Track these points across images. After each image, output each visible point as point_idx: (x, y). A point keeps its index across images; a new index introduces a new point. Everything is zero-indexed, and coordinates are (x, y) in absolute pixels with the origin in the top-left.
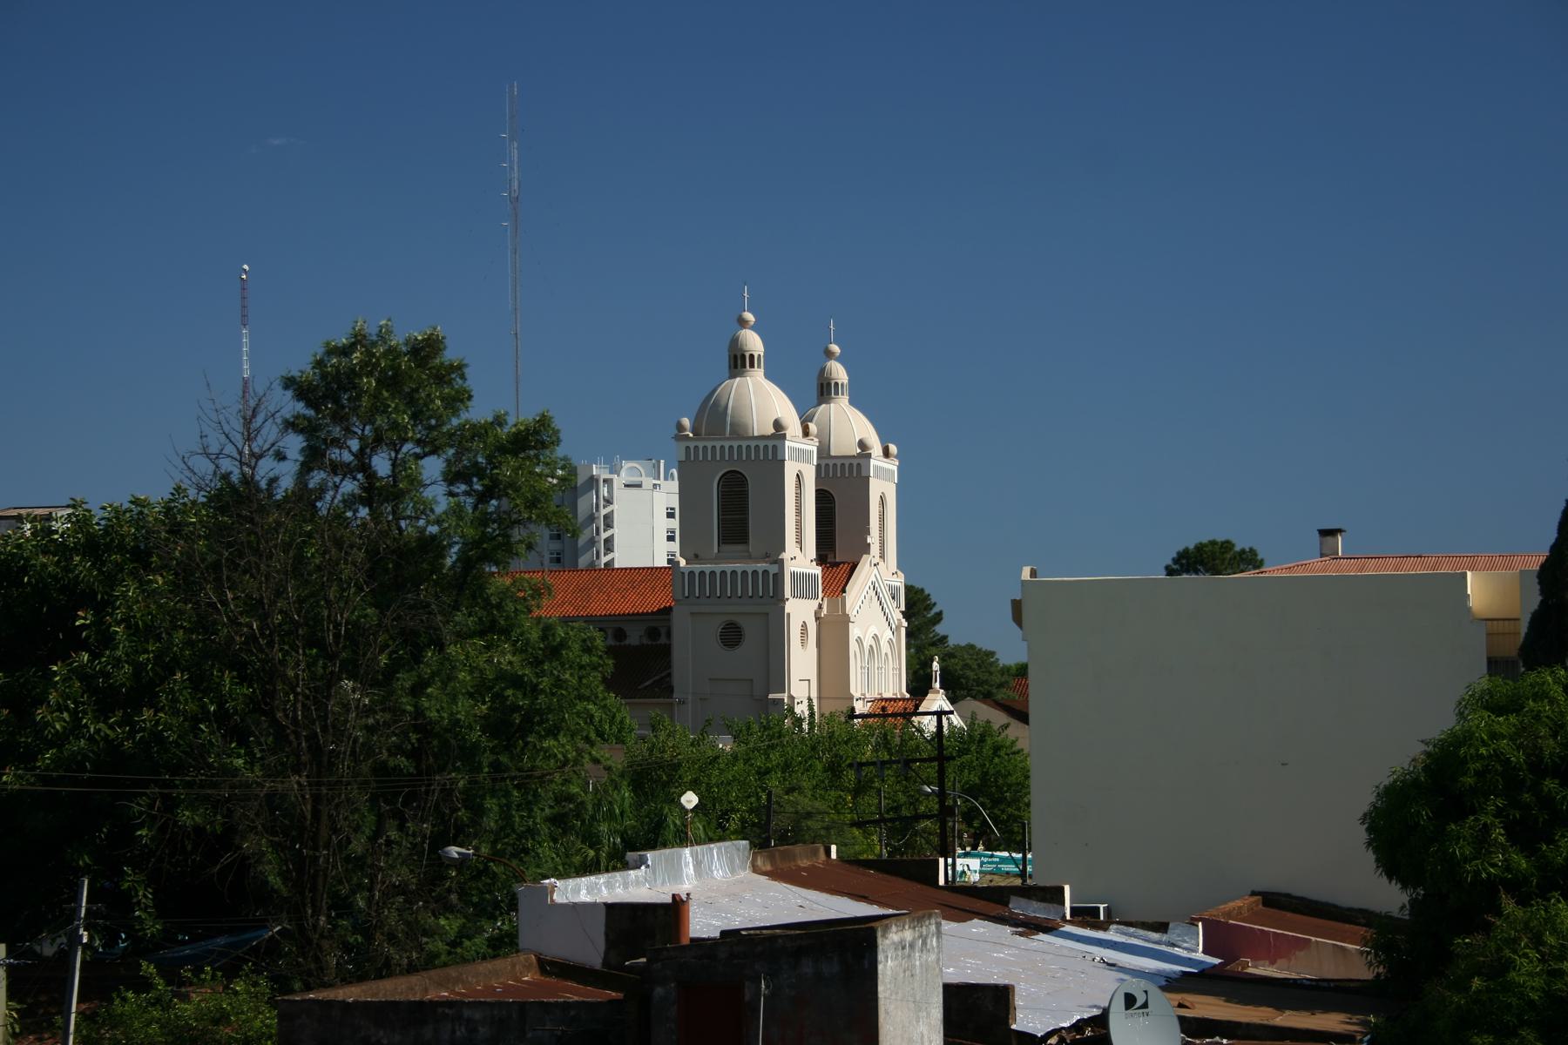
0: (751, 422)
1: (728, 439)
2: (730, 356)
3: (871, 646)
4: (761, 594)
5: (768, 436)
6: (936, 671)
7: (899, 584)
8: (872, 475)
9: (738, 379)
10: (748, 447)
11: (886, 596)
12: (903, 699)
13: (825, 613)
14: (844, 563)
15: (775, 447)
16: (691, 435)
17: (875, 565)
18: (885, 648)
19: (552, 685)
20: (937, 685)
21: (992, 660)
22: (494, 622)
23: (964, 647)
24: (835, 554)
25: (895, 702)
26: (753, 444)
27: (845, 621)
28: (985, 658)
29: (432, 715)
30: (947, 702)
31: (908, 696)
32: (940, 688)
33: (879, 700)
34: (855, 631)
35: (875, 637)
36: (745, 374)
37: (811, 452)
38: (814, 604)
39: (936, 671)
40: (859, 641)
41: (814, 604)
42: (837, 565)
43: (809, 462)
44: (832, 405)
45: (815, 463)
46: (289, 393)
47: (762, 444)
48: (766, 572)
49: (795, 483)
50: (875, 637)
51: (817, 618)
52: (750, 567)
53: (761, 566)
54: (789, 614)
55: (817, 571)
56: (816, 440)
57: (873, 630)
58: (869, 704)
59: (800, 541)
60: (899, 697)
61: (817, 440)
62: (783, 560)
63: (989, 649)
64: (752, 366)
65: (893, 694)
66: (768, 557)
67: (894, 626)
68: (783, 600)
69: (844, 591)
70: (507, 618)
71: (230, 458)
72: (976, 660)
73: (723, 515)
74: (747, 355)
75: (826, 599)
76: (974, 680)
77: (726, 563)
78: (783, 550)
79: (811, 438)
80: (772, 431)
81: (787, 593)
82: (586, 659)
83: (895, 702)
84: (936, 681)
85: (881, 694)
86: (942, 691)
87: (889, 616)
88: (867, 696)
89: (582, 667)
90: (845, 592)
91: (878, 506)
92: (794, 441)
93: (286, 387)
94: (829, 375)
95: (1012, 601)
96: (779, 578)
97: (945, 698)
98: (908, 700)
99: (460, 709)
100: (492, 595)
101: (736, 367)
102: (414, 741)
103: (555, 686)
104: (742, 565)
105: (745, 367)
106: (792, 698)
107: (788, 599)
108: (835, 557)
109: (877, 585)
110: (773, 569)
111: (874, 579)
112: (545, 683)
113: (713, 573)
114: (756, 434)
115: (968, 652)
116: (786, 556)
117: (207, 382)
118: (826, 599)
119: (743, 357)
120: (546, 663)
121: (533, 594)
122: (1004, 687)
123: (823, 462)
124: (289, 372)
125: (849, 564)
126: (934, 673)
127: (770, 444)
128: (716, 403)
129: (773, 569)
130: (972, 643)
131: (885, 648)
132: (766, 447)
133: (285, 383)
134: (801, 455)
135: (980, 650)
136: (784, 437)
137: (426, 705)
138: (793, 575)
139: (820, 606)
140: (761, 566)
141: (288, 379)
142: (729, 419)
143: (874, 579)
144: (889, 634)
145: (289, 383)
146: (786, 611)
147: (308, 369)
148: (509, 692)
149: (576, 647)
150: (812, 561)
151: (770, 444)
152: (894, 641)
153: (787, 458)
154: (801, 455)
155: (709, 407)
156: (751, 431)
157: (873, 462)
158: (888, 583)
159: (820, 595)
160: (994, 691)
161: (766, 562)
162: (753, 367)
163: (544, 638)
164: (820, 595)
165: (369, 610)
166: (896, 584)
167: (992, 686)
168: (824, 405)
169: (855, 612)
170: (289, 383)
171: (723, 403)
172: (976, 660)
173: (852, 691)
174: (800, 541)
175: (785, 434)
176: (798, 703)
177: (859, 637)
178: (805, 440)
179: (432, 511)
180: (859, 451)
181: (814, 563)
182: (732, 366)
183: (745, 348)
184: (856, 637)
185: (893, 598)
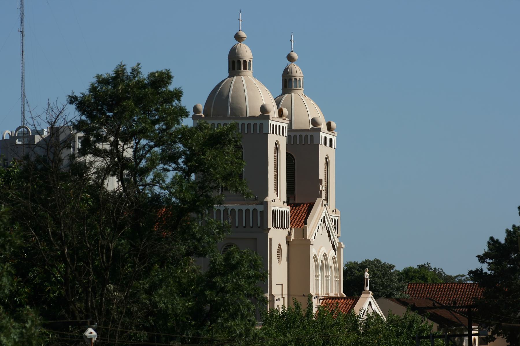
0: (245, 107)
1: (230, 119)
2: (229, 61)
3: (322, 261)
4: (251, 225)
5: (257, 117)
6: (367, 279)
7: (337, 218)
8: (321, 143)
9: (235, 77)
10: (243, 124)
11: (331, 225)
12: (342, 298)
13: (293, 238)
14: (304, 204)
15: (261, 124)
16: (203, 116)
17: (325, 205)
18: (331, 263)
19: (234, 288)
20: (368, 288)
21: (392, 271)
22: (196, 248)
23: (372, 262)
24: (295, 196)
25: (339, 300)
26: (246, 122)
27: (307, 244)
28: (388, 269)
29: (161, 306)
30: (374, 299)
31: (345, 295)
32: (370, 290)
33: (327, 299)
34: (313, 251)
35: (325, 255)
36: (241, 74)
37: (284, 128)
38: (285, 232)
39: (367, 279)
40: (315, 257)
41: (285, 232)
42: (299, 205)
43: (283, 134)
44: (293, 94)
45: (287, 135)
46: (74, 106)
47: (252, 122)
48: (255, 210)
49: (274, 149)
50: (325, 255)
51: (288, 242)
52: (244, 207)
53: (251, 206)
54: (271, 239)
55: (288, 209)
56: (287, 119)
57: (323, 250)
58: (321, 301)
59: (277, 190)
60: (339, 296)
61: (288, 120)
62: (267, 202)
63: (390, 263)
64: (245, 68)
65: (335, 294)
66: (256, 200)
67: (336, 248)
68: (268, 230)
69: (305, 223)
70: (203, 247)
71: (40, 147)
72: (381, 271)
73: (293, 181)
74: (242, 61)
75: (293, 229)
76: (380, 285)
77: (232, 204)
78: (267, 195)
79: (285, 118)
80: (258, 113)
81: (270, 225)
82: (252, 272)
83: (339, 300)
84: (367, 286)
85: (328, 294)
86: (371, 292)
87: (333, 241)
88: (320, 295)
89: (249, 277)
90: (306, 224)
91: (324, 164)
92: (274, 121)
93: (71, 103)
94: (290, 74)
95: (492, 238)
96: (264, 214)
97: (372, 296)
98: (344, 298)
99: (178, 302)
100: (197, 232)
101: (234, 69)
102: (151, 321)
103: (236, 289)
104: (239, 205)
105: (240, 69)
106: (272, 296)
107: (270, 229)
108: (295, 200)
109: (326, 219)
110: (260, 208)
111: (324, 215)
112: (229, 286)
113: (240, 210)
114: (248, 116)
115: (375, 265)
116: (269, 199)
117: (49, 103)
118: (293, 229)
119: (239, 62)
120: (229, 275)
121: (219, 231)
122: (400, 290)
123: (292, 134)
124: (74, 93)
125: (307, 204)
126: (365, 280)
127: (258, 122)
128: (221, 93)
129: (260, 208)
130: (378, 258)
131: (331, 263)
132: (255, 124)
133: (71, 100)
134: (278, 130)
135: (384, 264)
136: (268, 118)
137: (157, 299)
138: (273, 212)
139: (289, 234)
140: (251, 206)
141: (73, 97)
142: (230, 105)
143: (324, 215)
144: (332, 253)
145: (73, 99)
146: (269, 237)
147: (87, 92)
148: (207, 293)
149: (246, 265)
150: (284, 202)
151: (258, 122)
152: (336, 257)
153: (270, 132)
154: (278, 130)
155: (216, 96)
156: (242, 114)
157: (321, 134)
158: (332, 217)
159: (290, 226)
160: (395, 293)
161: (255, 203)
162: (246, 69)
163: (226, 259)
164: (290, 226)
165: (123, 241)
166: (335, 218)
167: (392, 289)
168: (287, 95)
169: (313, 238)
170: (73, 99)
171: (225, 94)
172: (381, 271)
173: (311, 292)
174: (277, 190)
175: (269, 116)
176: (277, 300)
177: (325, 253)
178: (280, 120)
179: (164, 181)
180: (311, 126)
181: (286, 204)
182: (231, 69)
183: (242, 56)
184: (313, 255)
185: (335, 228)
